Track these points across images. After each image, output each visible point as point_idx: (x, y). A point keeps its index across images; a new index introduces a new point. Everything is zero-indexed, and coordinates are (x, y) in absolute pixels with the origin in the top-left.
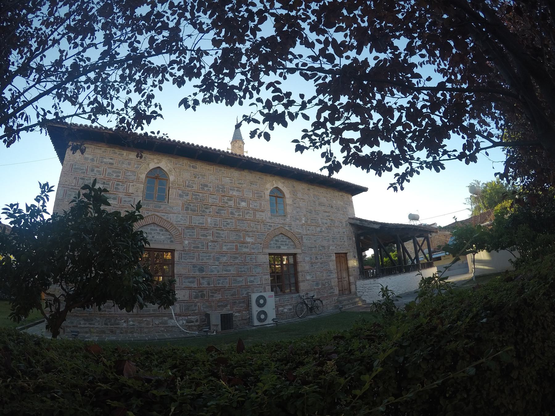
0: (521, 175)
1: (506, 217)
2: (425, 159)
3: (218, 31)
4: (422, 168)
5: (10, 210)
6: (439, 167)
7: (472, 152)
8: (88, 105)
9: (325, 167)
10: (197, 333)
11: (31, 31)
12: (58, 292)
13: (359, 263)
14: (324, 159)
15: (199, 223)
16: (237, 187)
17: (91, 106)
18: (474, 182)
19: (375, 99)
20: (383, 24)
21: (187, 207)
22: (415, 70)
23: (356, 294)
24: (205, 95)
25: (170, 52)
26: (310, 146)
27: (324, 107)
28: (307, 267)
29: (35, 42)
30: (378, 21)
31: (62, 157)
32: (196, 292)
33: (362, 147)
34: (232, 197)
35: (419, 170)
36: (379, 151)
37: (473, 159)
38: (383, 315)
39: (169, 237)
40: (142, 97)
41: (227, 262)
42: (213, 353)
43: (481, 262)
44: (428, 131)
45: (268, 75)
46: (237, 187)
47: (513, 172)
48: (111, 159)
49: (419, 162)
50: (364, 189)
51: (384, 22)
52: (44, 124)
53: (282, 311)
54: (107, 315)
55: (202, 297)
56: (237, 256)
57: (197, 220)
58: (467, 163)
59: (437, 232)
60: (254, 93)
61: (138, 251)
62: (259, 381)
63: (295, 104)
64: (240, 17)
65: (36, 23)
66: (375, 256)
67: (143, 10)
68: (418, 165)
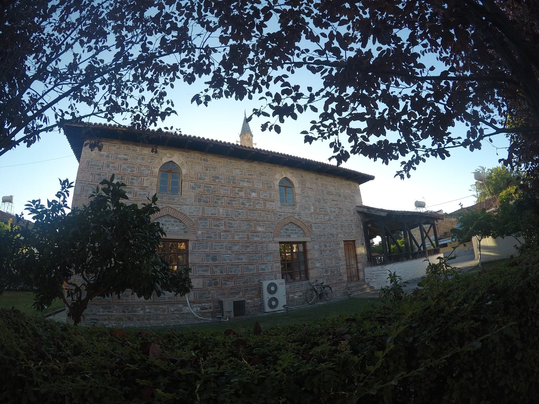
0: (526, 161)
1: (511, 203)
2: (431, 147)
3: (225, 28)
4: (428, 156)
5: (32, 206)
6: (444, 154)
7: (476, 139)
8: (104, 105)
9: (333, 157)
10: (211, 319)
11: (44, 37)
13: (367, 250)
14: (333, 149)
15: (211, 214)
16: (247, 179)
17: (107, 105)
18: (479, 168)
19: (379, 89)
20: (384, 16)
21: (199, 199)
22: (419, 60)
23: (364, 280)
24: (215, 90)
25: (180, 51)
26: (319, 137)
27: (331, 98)
28: (316, 255)
29: (48, 47)
30: (380, 12)
31: (78, 155)
32: (209, 280)
33: (368, 136)
34: (243, 188)
35: (425, 157)
36: (385, 140)
37: (477, 145)
38: (391, 300)
39: (183, 228)
40: (155, 94)
41: (239, 250)
42: (231, 336)
43: (487, 248)
44: (432, 119)
45: (277, 69)
46: (247, 179)
47: (517, 158)
48: (126, 155)
49: (425, 150)
50: (371, 178)
51: (385, 13)
52: (62, 124)
53: (293, 298)
54: (125, 303)
55: (215, 285)
56: (249, 244)
57: (209, 211)
58: (472, 149)
59: (443, 219)
60: (264, 87)
61: (155, 242)
62: (278, 359)
63: (303, 97)
64: (245, 14)
65: (49, 29)
66: (382, 244)
67: (152, 12)
68: (424, 153)
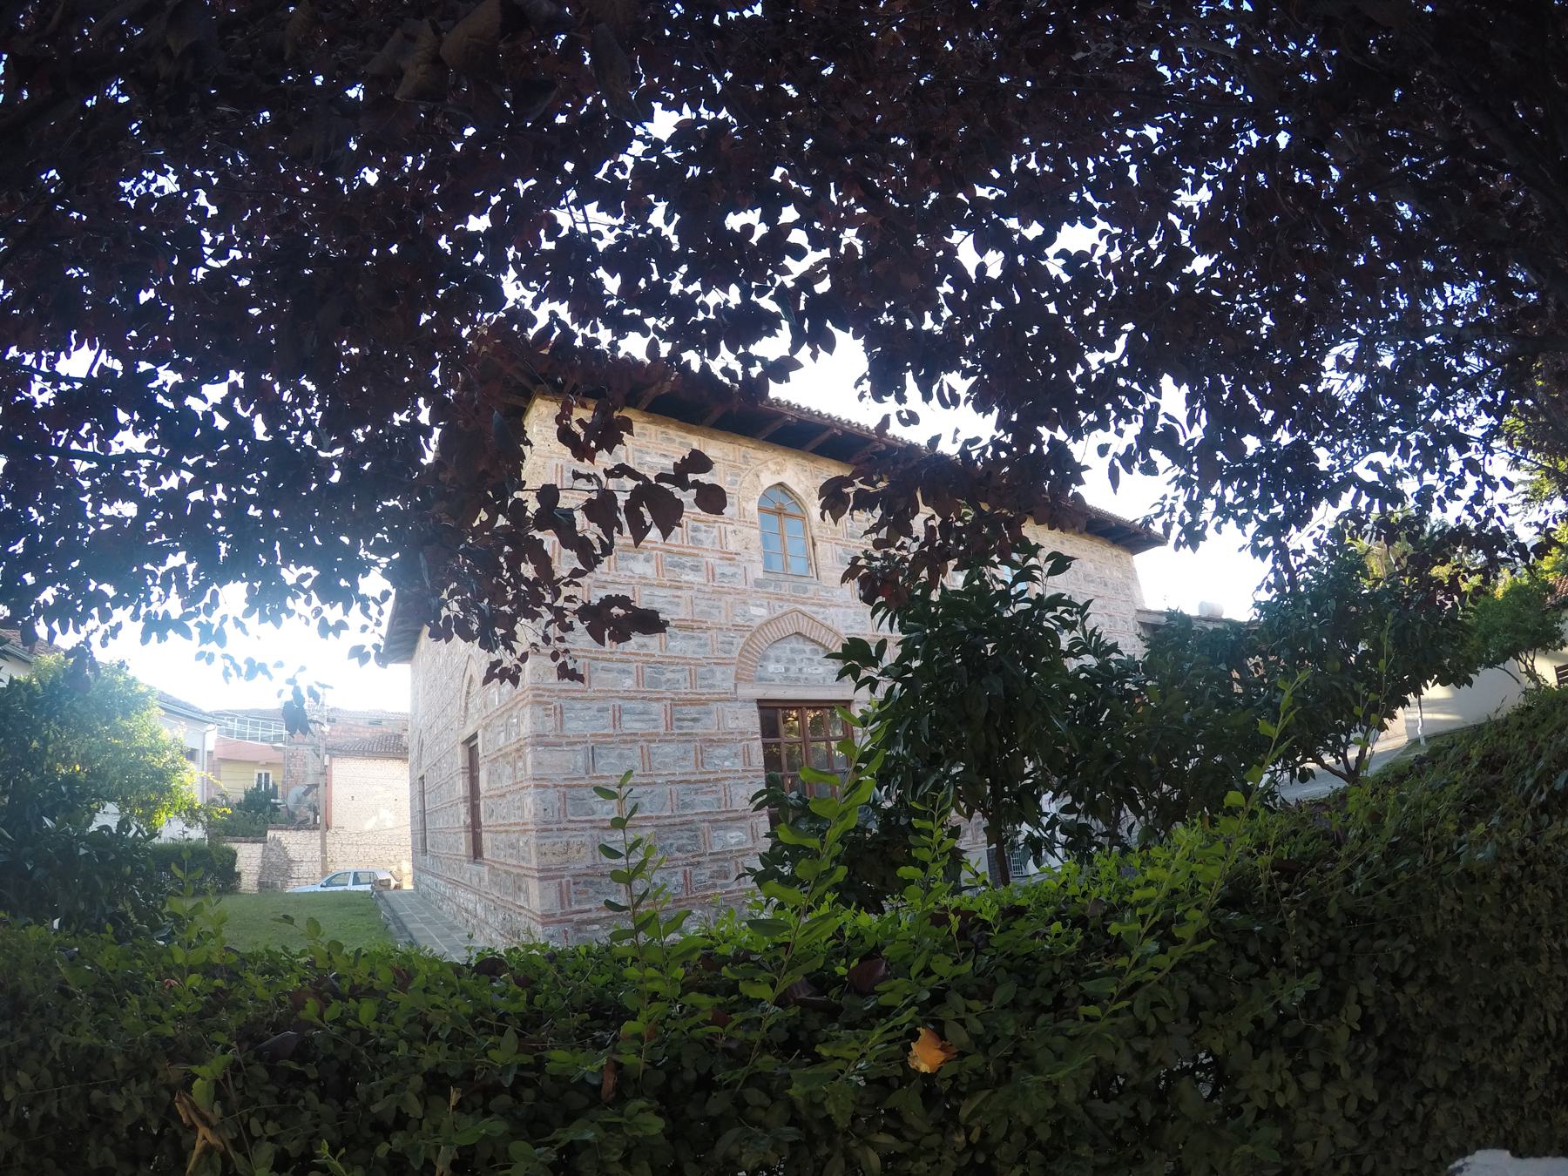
12: (579, 852)
48: (665, 456)
